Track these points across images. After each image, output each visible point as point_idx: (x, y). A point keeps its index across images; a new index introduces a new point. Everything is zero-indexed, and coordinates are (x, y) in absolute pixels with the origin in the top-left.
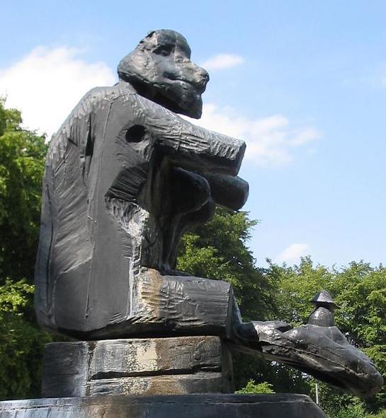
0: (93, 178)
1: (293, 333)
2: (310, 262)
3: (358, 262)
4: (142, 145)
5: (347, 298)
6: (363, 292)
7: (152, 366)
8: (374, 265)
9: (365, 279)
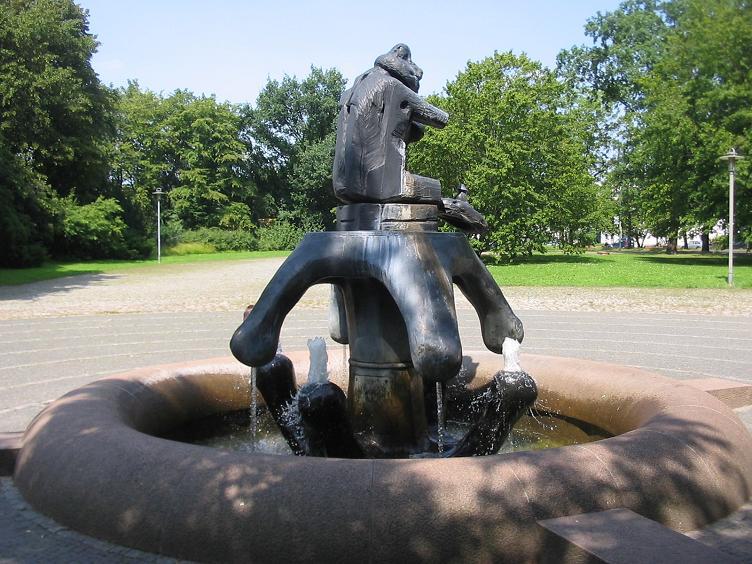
0: (385, 124)
1: (458, 205)
2: (137, 85)
3: (182, 90)
4: (406, 111)
5: (173, 124)
6: (189, 119)
7: (409, 218)
8: (198, 94)
9: (189, 107)
